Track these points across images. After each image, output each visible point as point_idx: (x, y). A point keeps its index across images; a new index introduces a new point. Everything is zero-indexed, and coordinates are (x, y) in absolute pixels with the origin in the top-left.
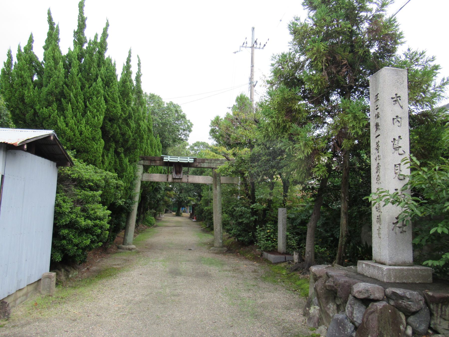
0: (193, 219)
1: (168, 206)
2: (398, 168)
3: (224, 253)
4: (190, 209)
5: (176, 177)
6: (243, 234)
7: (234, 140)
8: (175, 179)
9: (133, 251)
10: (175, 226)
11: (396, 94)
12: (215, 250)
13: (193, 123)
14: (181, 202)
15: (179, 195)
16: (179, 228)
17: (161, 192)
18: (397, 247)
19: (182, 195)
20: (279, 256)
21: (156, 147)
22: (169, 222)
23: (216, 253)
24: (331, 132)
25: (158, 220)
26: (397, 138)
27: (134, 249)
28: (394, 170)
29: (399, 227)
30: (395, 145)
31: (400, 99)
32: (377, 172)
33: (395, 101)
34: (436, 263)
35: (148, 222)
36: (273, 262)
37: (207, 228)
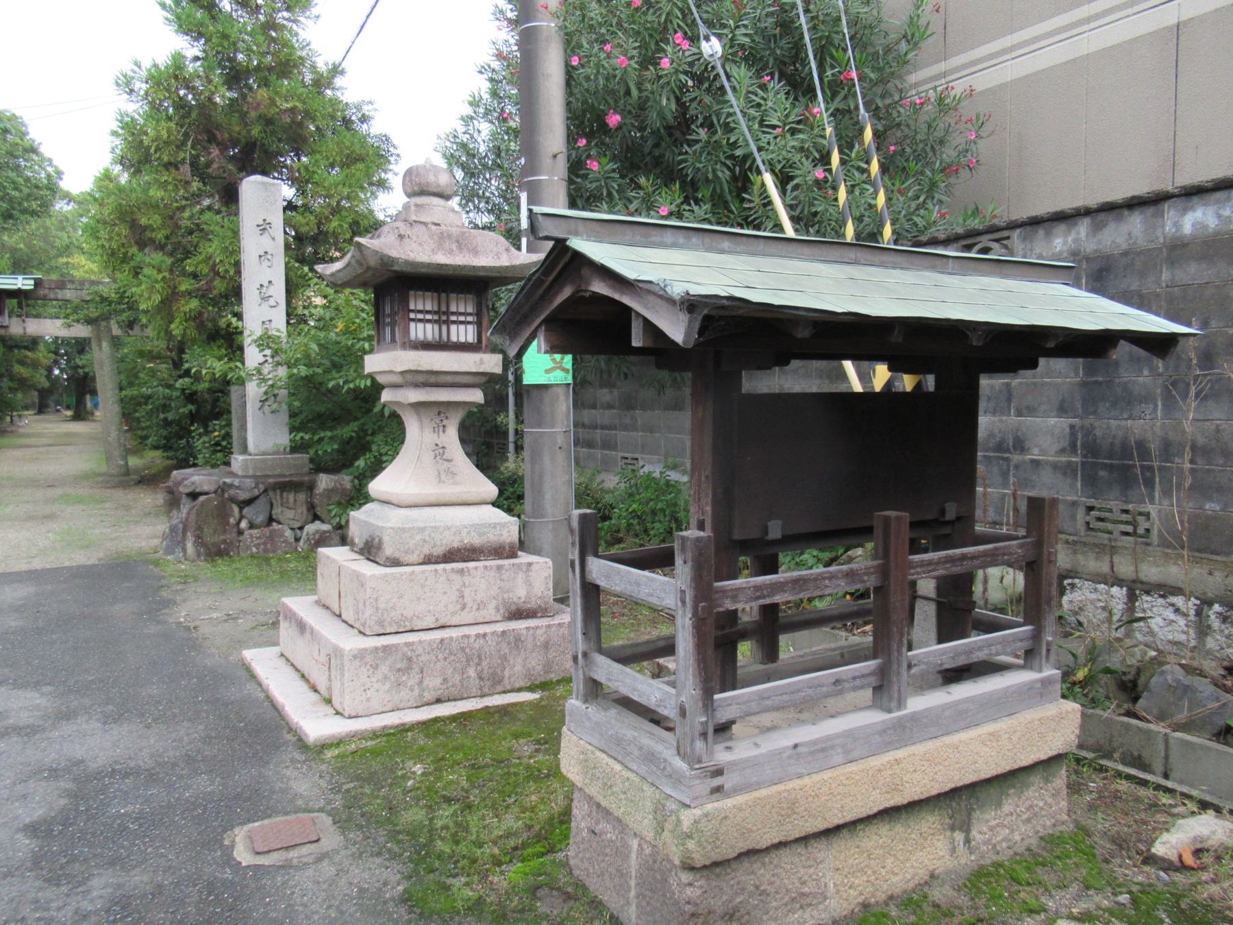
13: (61, 168)
22: (39, 435)
23: (113, 487)
26: (266, 284)
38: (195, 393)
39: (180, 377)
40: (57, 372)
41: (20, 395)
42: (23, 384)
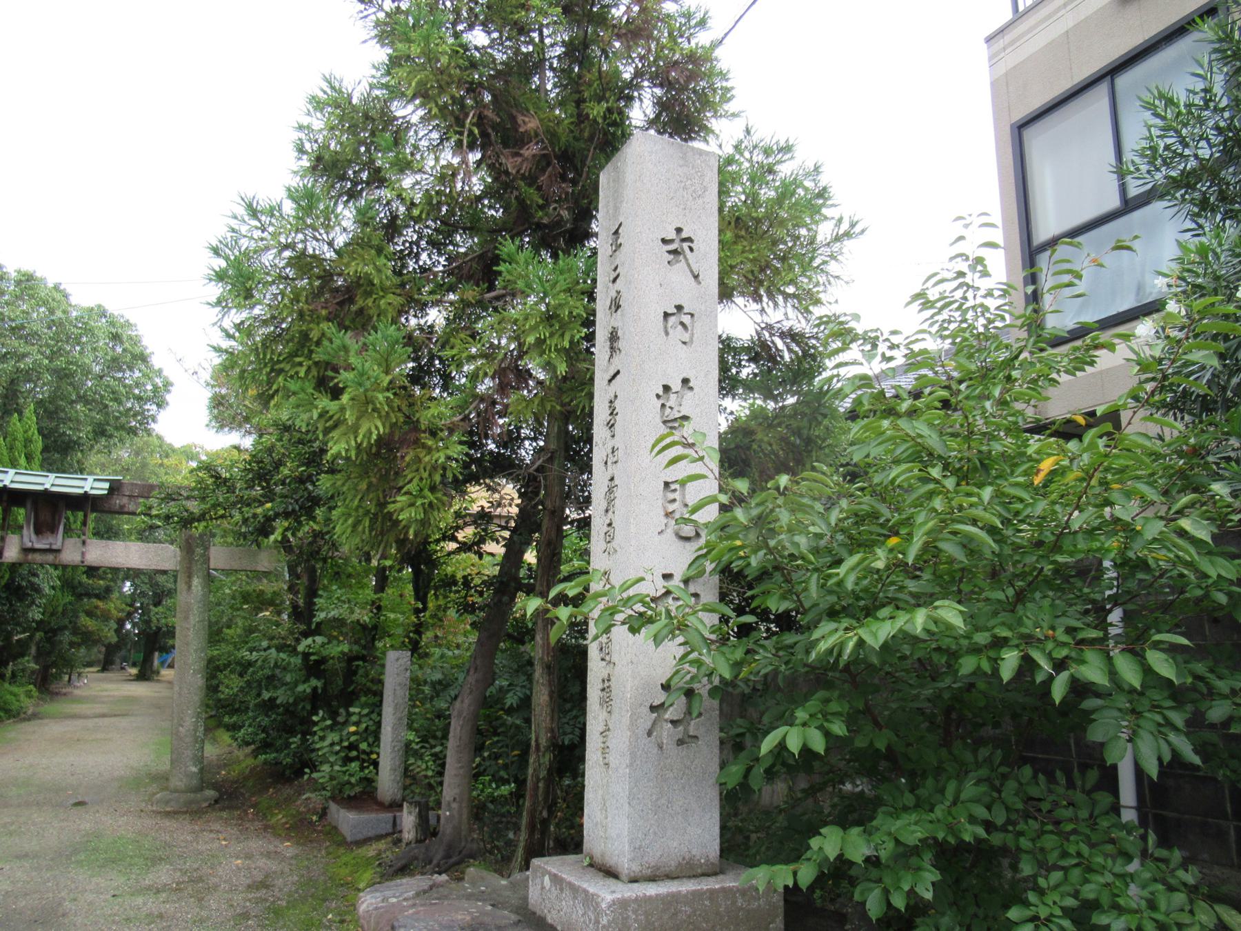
2: (676, 495)
3: (193, 812)
5: (37, 546)
10: (104, 716)
11: (679, 230)
12: (167, 802)
13: (171, 379)
16: (107, 720)
18: (663, 801)
20: (373, 816)
21: (19, 445)
23: (168, 814)
24: (268, 258)
26: (676, 385)
28: (660, 502)
29: (672, 722)
30: (668, 411)
31: (691, 249)
32: (607, 511)
33: (675, 252)
34: (783, 875)
36: (349, 839)
38: (323, 660)
39: (306, 635)
40: (128, 626)
41: (83, 650)
42: (88, 639)
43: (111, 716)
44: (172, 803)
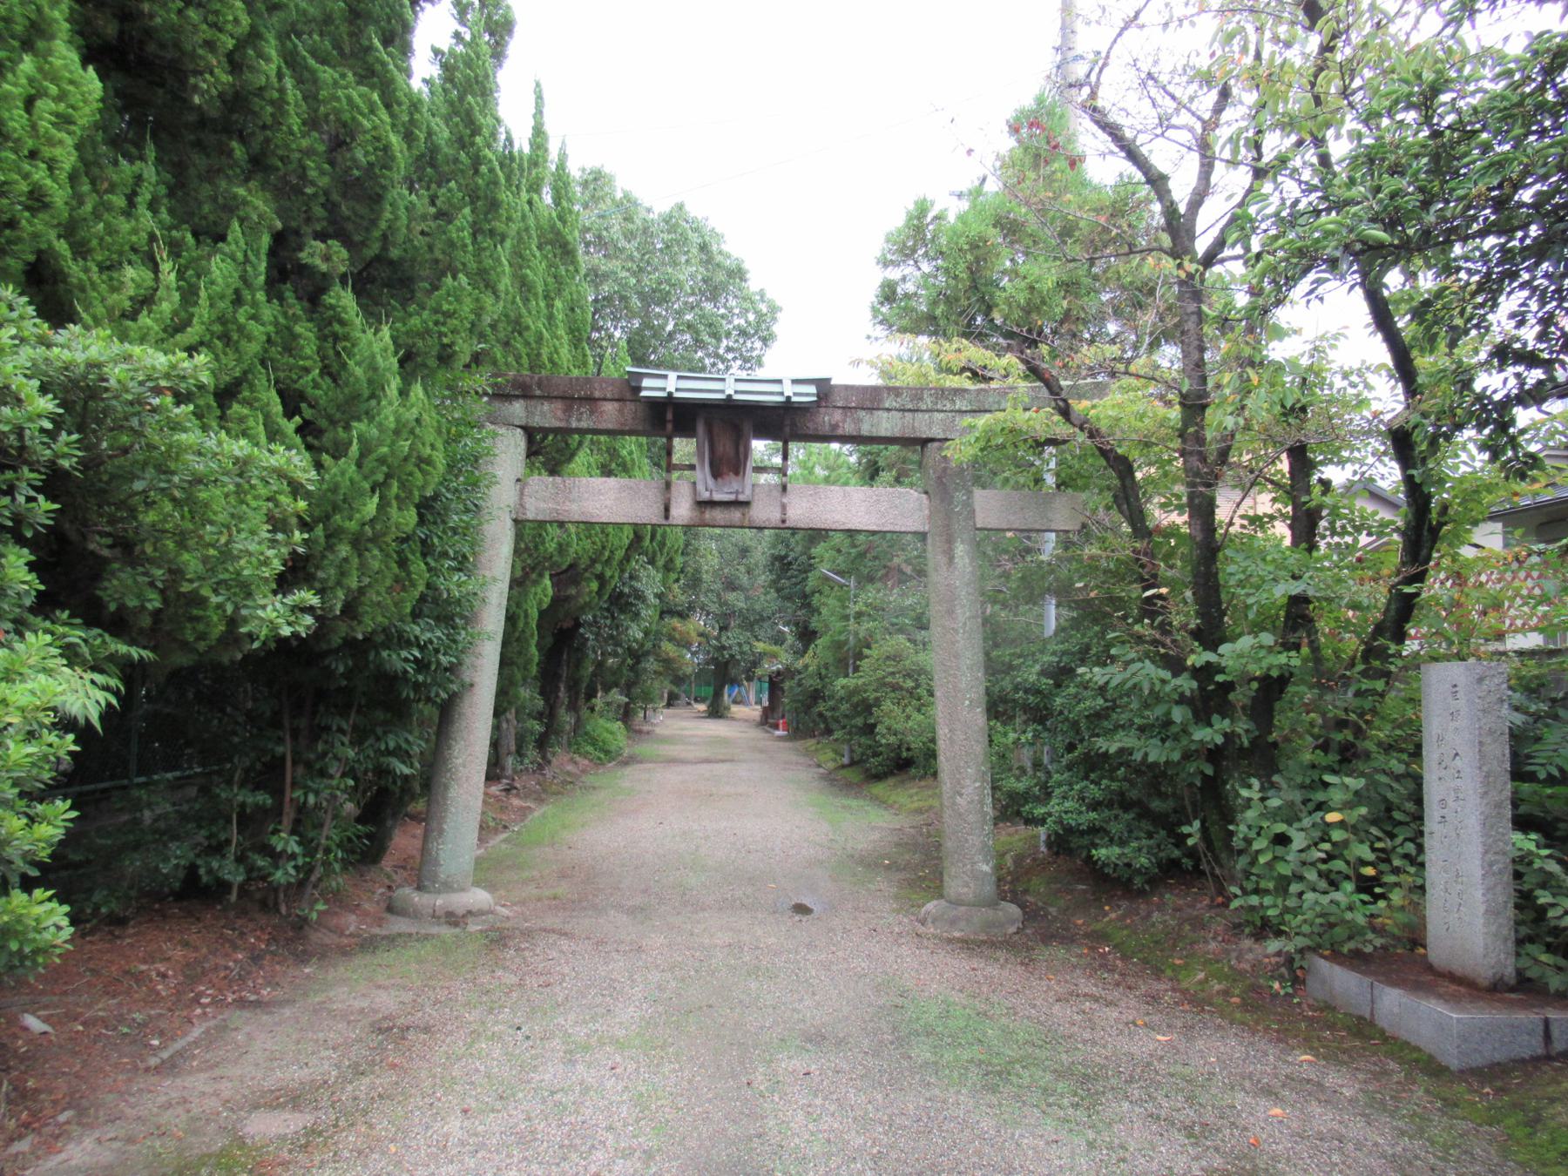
0: (776, 727)
1: (679, 680)
4: (760, 691)
5: (717, 497)
6: (1115, 828)
7: (1017, 314)
8: (712, 504)
9: (473, 927)
10: (707, 761)
13: (778, 303)
14: (727, 663)
15: (718, 639)
17: (643, 613)
19: (733, 638)
25: (640, 732)
27: (481, 913)
35: (593, 742)
37: (843, 766)
43: (723, 761)
44: (962, 924)
